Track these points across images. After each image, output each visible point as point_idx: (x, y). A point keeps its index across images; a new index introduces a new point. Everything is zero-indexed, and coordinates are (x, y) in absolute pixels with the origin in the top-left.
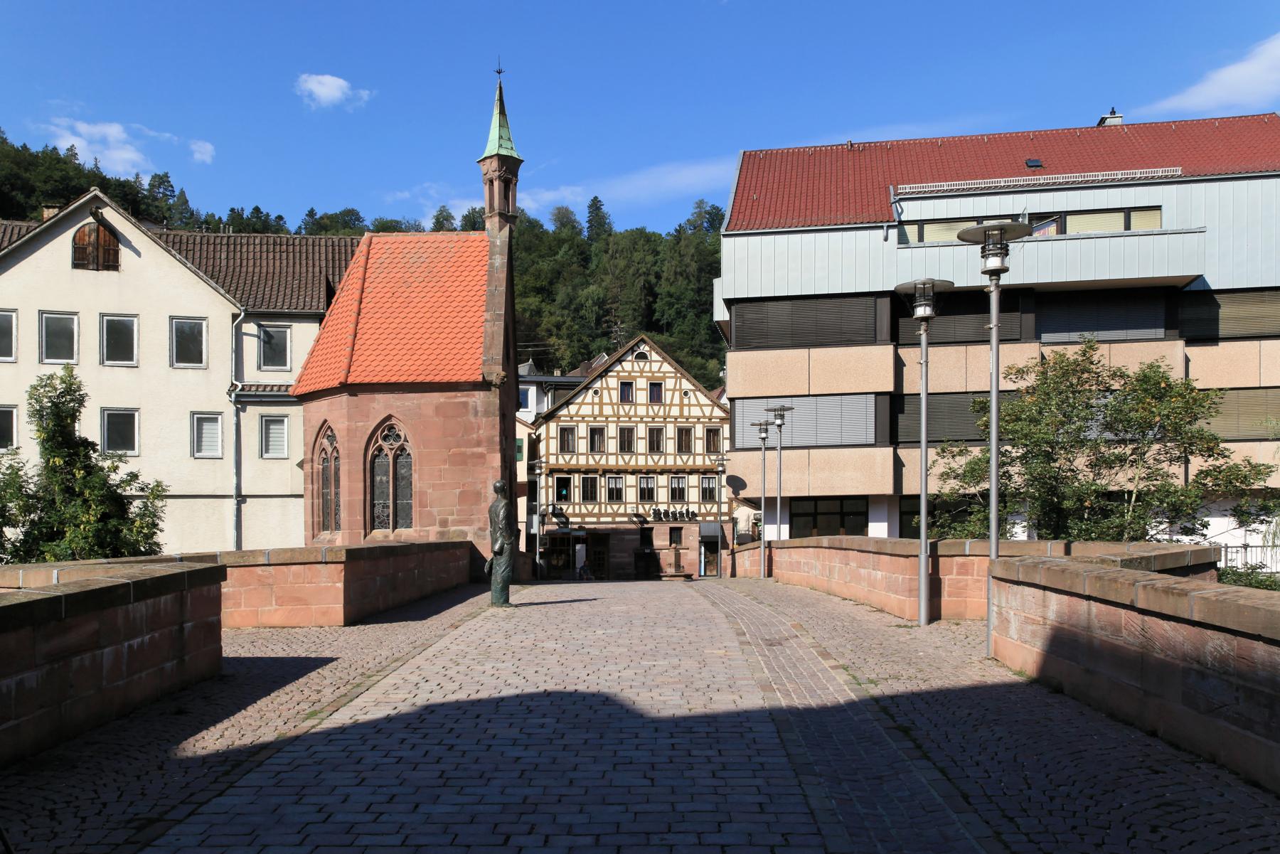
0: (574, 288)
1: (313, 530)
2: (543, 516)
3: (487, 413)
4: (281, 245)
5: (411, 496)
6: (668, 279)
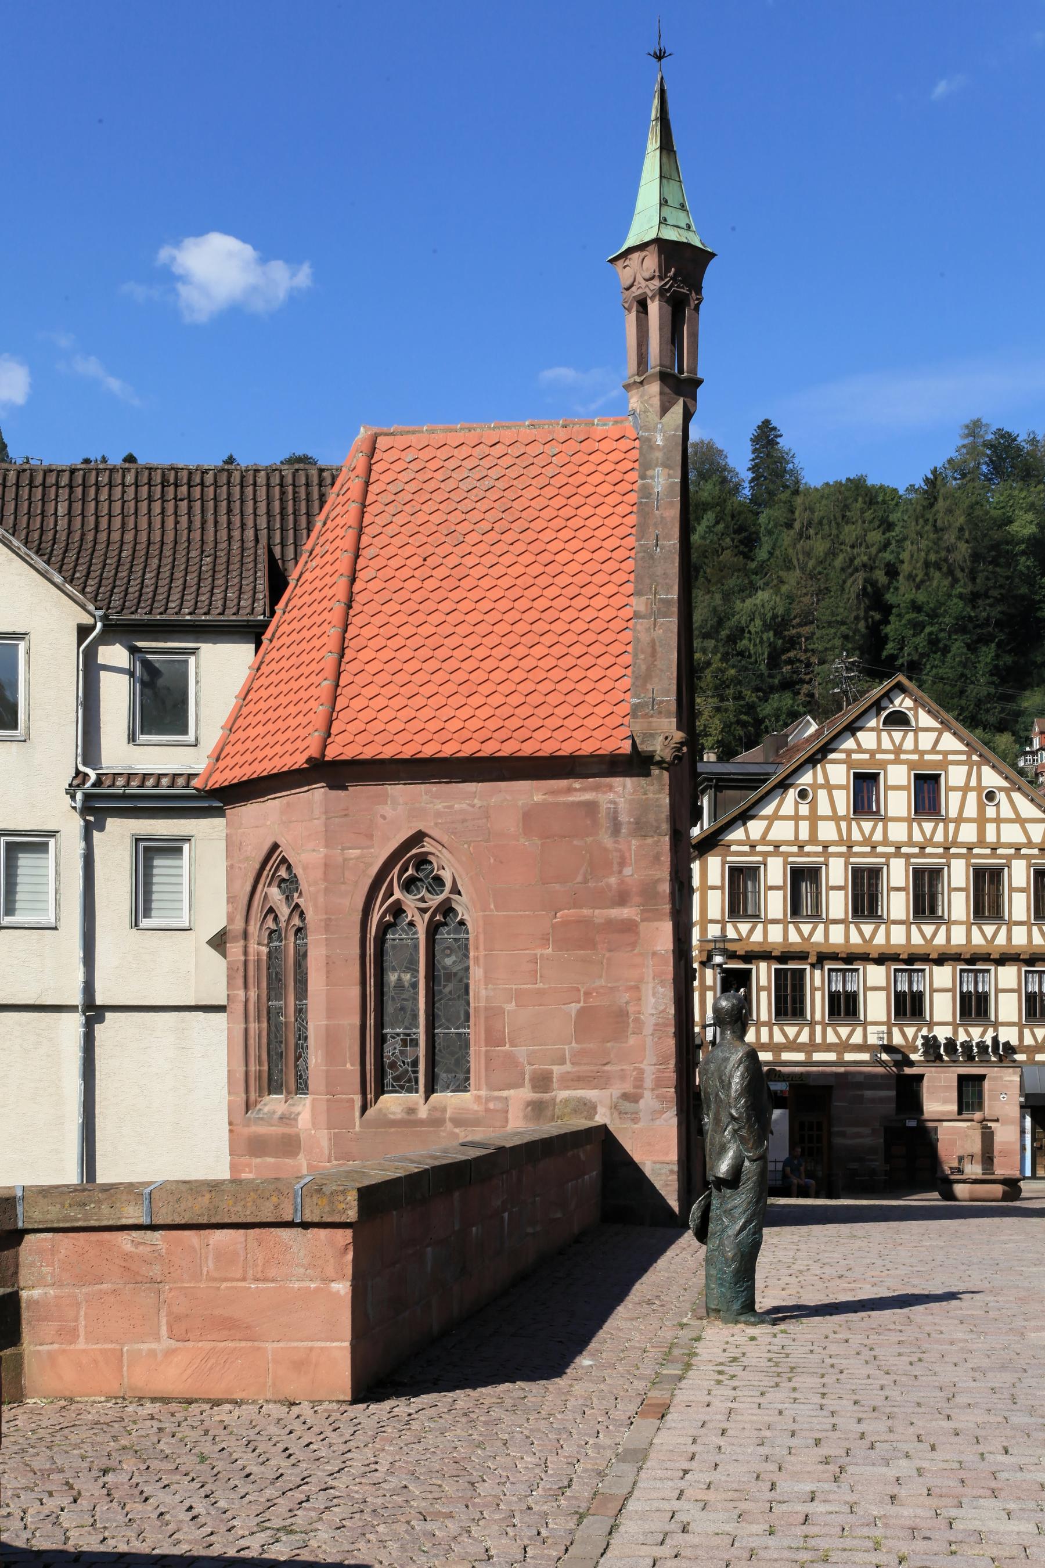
0: (727, 597)
1: (247, 1091)
3: (640, 828)
4: (176, 486)
6: (911, 577)
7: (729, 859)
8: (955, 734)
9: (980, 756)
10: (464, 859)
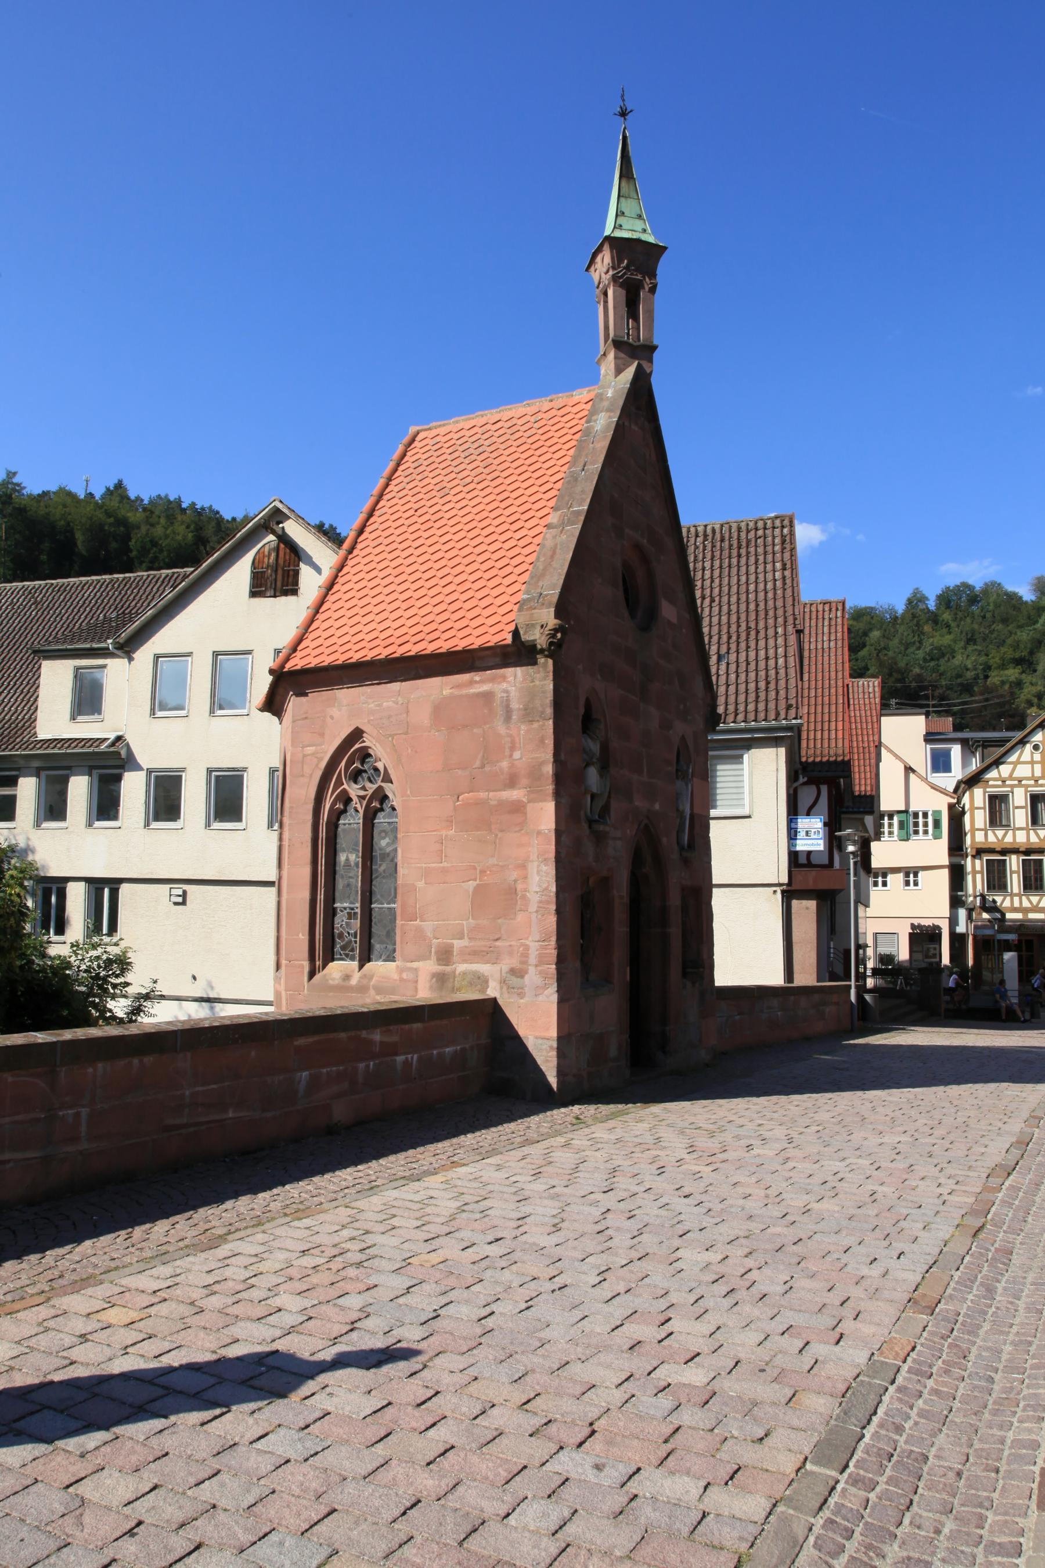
2: (970, 911)
3: (529, 714)
5: (396, 897)
7: (988, 790)
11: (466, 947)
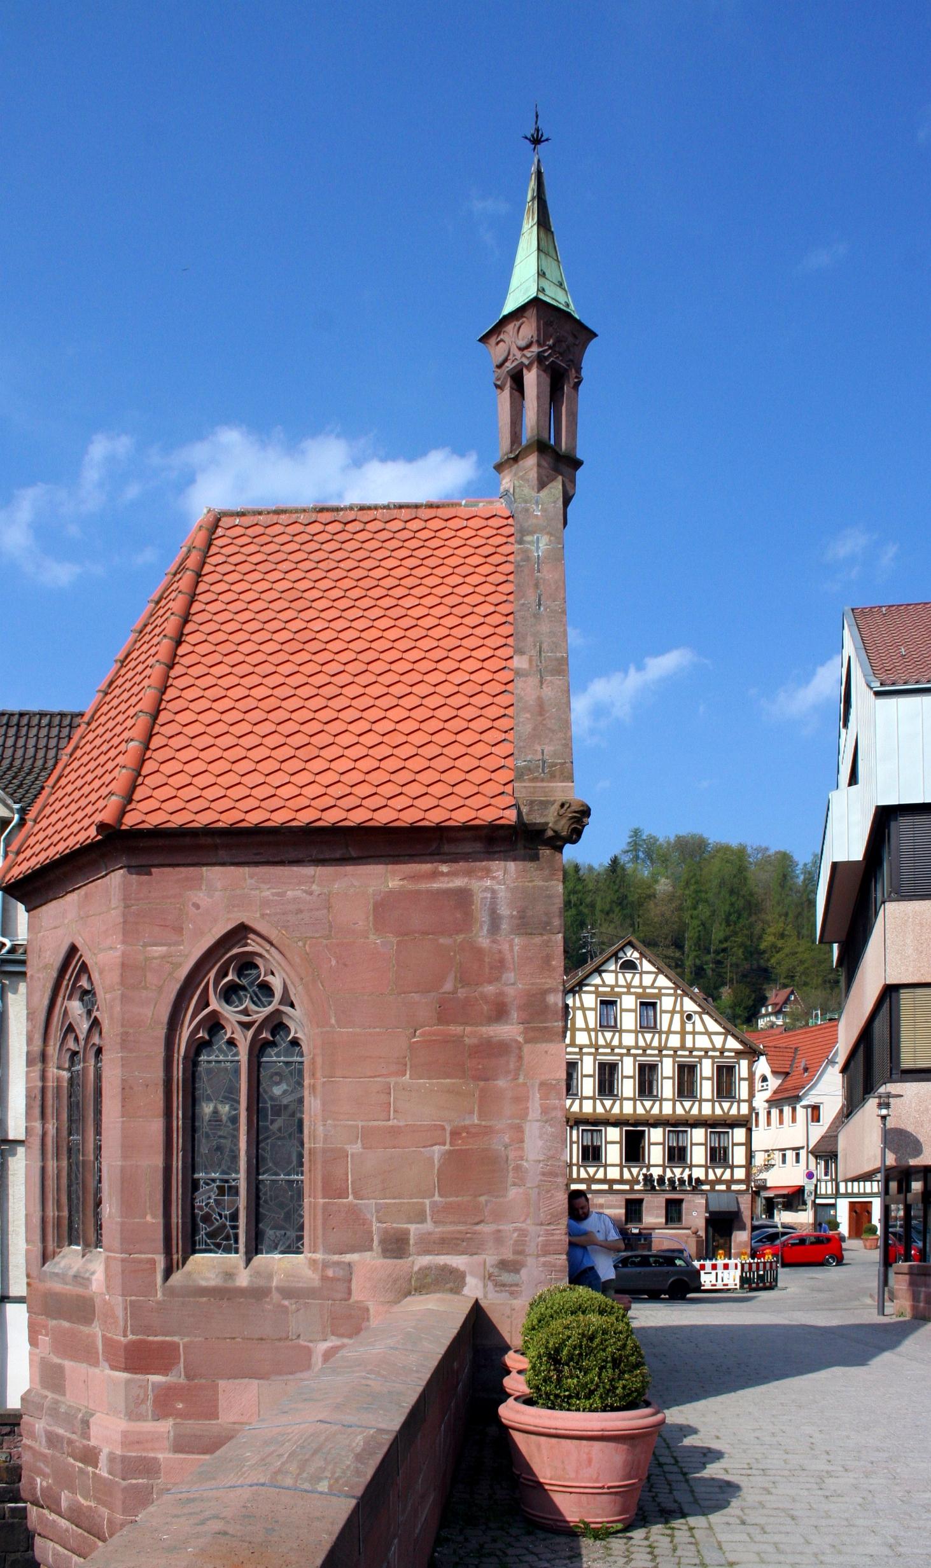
1: (44, 1239)
3: (525, 925)
5: (301, 1164)
8: (666, 976)
9: (682, 991)
10: (297, 960)
11: (430, 1234)
